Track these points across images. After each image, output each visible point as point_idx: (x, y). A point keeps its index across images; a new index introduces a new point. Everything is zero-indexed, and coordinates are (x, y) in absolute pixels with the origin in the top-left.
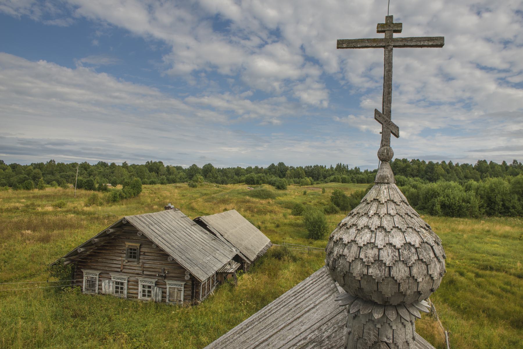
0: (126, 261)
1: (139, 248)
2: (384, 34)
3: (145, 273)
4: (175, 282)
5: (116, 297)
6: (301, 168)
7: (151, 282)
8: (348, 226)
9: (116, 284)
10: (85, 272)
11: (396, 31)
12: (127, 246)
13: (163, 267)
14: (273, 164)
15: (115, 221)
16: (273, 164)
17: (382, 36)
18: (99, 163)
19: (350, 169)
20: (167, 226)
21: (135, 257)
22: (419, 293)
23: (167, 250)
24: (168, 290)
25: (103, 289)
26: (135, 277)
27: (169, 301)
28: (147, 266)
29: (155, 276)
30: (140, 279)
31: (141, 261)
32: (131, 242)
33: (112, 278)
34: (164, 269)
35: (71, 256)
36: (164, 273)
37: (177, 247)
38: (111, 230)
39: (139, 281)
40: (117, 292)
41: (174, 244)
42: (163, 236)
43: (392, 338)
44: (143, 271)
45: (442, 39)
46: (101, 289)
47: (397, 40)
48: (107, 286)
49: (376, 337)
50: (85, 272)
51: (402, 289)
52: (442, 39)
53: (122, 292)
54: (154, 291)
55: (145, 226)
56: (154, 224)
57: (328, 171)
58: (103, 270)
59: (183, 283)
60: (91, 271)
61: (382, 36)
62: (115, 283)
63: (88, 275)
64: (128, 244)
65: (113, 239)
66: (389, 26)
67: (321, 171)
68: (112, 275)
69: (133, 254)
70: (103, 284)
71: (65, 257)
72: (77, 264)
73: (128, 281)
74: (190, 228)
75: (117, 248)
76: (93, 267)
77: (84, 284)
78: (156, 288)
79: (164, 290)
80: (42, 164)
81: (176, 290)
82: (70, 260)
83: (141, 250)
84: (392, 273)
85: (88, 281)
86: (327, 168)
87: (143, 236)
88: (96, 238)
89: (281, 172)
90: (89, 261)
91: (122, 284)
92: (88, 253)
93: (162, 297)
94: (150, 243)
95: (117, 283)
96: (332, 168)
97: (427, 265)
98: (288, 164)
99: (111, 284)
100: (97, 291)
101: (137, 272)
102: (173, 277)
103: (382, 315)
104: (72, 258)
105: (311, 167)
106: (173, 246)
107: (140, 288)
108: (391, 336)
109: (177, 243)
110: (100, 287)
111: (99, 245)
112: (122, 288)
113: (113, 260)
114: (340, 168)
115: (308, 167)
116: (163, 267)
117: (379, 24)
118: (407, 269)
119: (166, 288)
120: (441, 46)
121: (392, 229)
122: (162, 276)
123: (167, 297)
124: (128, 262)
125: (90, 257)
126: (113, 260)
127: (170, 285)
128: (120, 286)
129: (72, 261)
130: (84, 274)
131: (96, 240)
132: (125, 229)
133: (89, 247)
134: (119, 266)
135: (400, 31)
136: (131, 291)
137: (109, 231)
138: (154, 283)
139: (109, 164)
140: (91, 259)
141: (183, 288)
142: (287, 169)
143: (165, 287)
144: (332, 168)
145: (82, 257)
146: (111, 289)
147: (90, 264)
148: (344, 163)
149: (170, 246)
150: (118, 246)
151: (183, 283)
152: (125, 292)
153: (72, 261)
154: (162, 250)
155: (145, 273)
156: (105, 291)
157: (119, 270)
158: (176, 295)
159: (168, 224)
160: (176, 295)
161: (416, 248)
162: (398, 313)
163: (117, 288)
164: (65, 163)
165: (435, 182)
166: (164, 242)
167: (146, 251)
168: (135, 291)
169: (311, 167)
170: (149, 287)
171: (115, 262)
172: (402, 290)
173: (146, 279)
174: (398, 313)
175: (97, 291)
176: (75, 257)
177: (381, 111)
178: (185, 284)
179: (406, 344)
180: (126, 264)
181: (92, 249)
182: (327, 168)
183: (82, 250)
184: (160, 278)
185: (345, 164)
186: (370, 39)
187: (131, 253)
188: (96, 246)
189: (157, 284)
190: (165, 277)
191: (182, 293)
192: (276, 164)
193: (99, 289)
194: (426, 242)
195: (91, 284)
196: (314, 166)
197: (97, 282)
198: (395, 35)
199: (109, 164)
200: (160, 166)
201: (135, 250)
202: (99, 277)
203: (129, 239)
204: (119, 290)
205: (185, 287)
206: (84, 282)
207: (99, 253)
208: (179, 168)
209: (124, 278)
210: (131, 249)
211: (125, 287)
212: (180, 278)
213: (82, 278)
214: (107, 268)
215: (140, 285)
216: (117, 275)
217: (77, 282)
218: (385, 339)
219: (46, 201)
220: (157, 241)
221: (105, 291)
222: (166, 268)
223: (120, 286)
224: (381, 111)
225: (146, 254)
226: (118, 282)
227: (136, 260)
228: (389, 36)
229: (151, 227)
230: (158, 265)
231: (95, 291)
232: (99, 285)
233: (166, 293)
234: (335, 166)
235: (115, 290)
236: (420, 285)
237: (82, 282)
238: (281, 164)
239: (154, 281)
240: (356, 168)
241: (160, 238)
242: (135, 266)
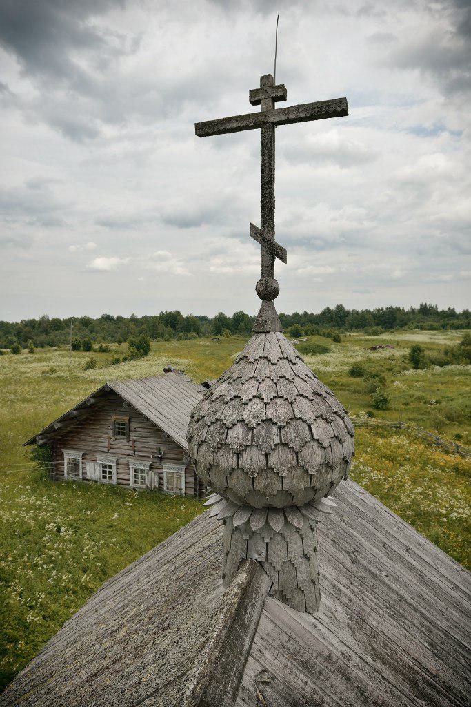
0: (114, 438)
1: (127, 422)
5: (103, 484)
6: (368, 312)
8: (214, 399)
10: (66, 452)
11: (275, 99)
14: (328, 309)
16: (328, 309)
17: (257, 109)
18: (103, 317)
21: (123, 434)
22: (315, 490)
24: (165, 474)
25: (88, 474)
27: (168, 489)
29: (149, 457)
30: (131, 460)
31: (131, 439)
32: (119, 415)
35: (49, 433)
36: (160, 453)
38: (92, 401)
40: (104, 477)
41: (170, 417)
45: (343, 101)
47: (282, 111)
48: (92, 470)
49: (243, 550)
50: (66, 452)
51: (258, 487)
52: (343, 101)
53: (110, 478)
55: (134, 395)
59: (184, 467)
60: (72, 452)
61: (257, 109)
63: (69, 455)
64: (114, 417)
67: (398, 315)
68: (98, 456)
69: (122, 430)
70: (88, 468)
72: (56, 440)
73: (117, 464)
75: (102, 422)
76: (75, 447)
77: (66, 468)
79: (161, 476)
82: (46, 438)
83: (131, 425)
84: (240, 462)
87: (130, 406)
88: (75, 410)
91: (110, 467)
92: (68, 429)
93: (159, 484)
95: (104, 466)
97: (297, 453)
98: (348, 307)
99: (97, 467)
101: (126, 452)
102: (171, 459)
105: (382, 309)
106: (168, 419)
107: (132, 473)
108: (264, 551)
110: (84, 471)
112: (110, 473)
114: (425, 311)
115: (378, 310)
118: (263, 458)
119: (163, 473)
120: (344, 113)
125: (71, 434)
127: (168, 469)
128: (107, 470)
129: (50, 439)
132: (107, 399)
133: (68, 422)
134: (105, 445)
135: (283, 98)
136: (121, 476)
138: (148, 466)
140: (72, 437)
142: (347, 313)
143: (161, 471)
146: (97, 473)
147: (70, 443)
148: (431, 302)
149: (164, 419)
150: (103, 420)
152: (114, 477)
153: (50, 439)
154: (155, 425)
157: (106, 450)
158: (175, 483)
159: (165, 391)
160: (175, 483)
161: (280, 428)
163: (104, 472)
164: (184, 314)
166: (157, 414)
167: (137, 426)
168: (125, 477)
169: (382, 309)
170: (142, 471)
171: (100, 440)
172: (259, 488)
177: (259, 226)
179: (288, 564)
180: (114, 443)
182: (406, 310)
183: (59, 425)
184: (155, 460)
186: (239, 117)
187: (119, 428)
189: (151, 467)
190: (161, 459)
191: (183, 479)
192: (333, 308)
193: (83, 474)
195: (74, 468)
197: (81, 465)
198: (279, 105)
201: (123, 424)
204: (107, 475)
205: (186, 472)
206: (65, 465)
207: (81, 428)
208: (203, 319)
209: (110, 460)
210: (119, 424)
211: (114, 470)
212: (178, 460)
215: (131, 469)
216: (103, 456)
218: (256, 556)
219: (30, 364)
220: (147, 413)
223: (107, 470)
224: (259, 226)
226: (106, 466)
228: (270, 110)
229: (142, 396)
230: (152, 444)
231: (78, 475)
232: (83, 469)
234: (417, 307)
237: (63, 465)
238: (340, 308)
239: (148, 464)
240: (449, 309)
241: (152, 409)
242: (123, 445)
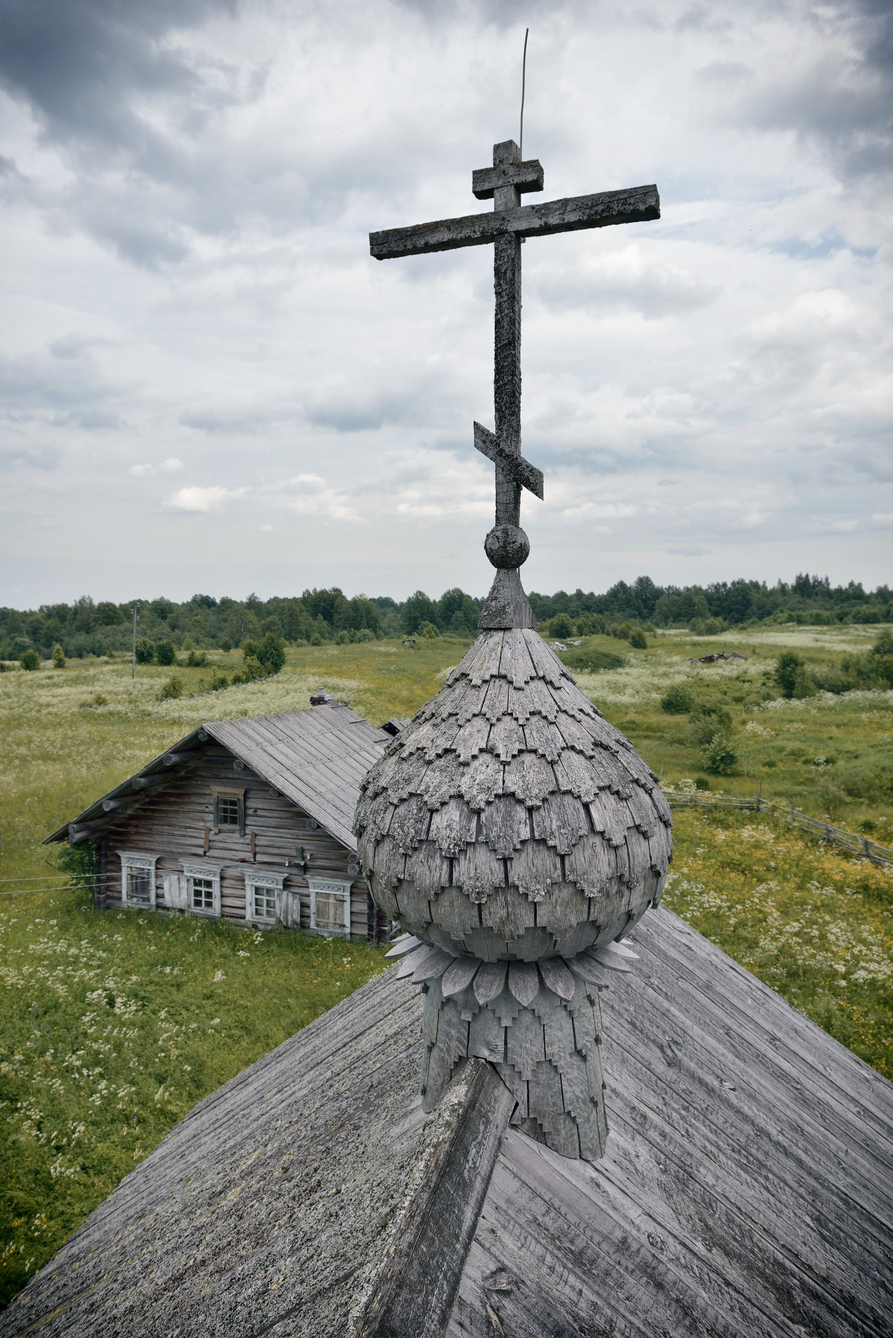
1: (242, 798)
2: (491, 201)
3: (259, 858)
4: (330, 882)
6: (697, 590)
9: (196, 884)
10: (124, 856)
12: (215, 795)
13: (300, 843)
15: (179, 735)
16: (622, 585)
17: (488, 206)
18: (194, 600)
19: (833, 586)
20: (308, 744)
21: (234, 821)
23: (306, 804)
25: (167, 896)
26: (237, 866)
27: (318, 925)
29: (283, 865)
30: (248, 871)
31: (248, 830)
33: (185, 869)
34: (303, 850)
35: (92, 819)
36: (304, 858)
37: (330, 796)
38: (175, 758)
39: (246, 878)
40: (198, 903)
42: (299, 772)
43: (501, 1048)
44: (255, 854)
45: (651, 191)
46: (162, 896)
48: (175, 888)
49: (461, 1042)
50: (124, 856)
52: (651, 191)
53: (209, 904)
54: (280, 900)
55: (254, 747)
56: (275, 740)
57: (772, 592)
58: (163, 851)
61: (488, 206)
62: (192, 881)
63: (131, 862)
64: (217, 790)
65: (184, 778)
66: (509, 172)
67: (755, 596)
69: (231, 814)
70: (166, 885)
71: (76, 823)
73: (222, 878)
74: (369, 749)
75: (193, 799)
76: (141, 845)
78: (285, 893)
79: (305, 900)
80: (64, 607)
81: (332, 901)
82: (88, 828)
84: (455, 875)
85: (132, 876)
87: (247, 769)
89: (644, 601)
90: (133, 830)
91: (209, 884)
92: (129, 812)
93: (302, 916)
94: (265, 786)
95: (198, 883)
97: (562, 857)
98: (660, 582)
99: (184, 884)
100: (153, 901)
101: (242, 855)
103: (500, 991)
104: (92, 823)
105: (725, 585)
106: (319, 794)
107: (250, 895)
109: (332, 786)
110: (160, 891)
111: (154, 794)
112: (209, 895)
113: (187, 827)
115: (717, 587)
116: (300, 843)
117: (475, 172)
118: (497, 867)
119: (308, 896)
120: (653, 213)
121: (474, 757)
122: (298, 866)
123: (312, 916)
124: (220, 832)
126: (187, 827)
130: (123, 860)
131: (142, 780)
132: (203, 755)
133: (129, 799)
135: (536, 186)
136: (229, 901)
137: (169, 758)
138: (281, 882)
139: (218, 601)
140: (136, 826)
141: (347, 894)
143: (305, 891)
145: (116, 821)
146: (184, 895)
147: (135, 838)
148: (816, 571)
149: (311, 793)
150: (194, 794)
152: (216, 902)
153: (94, 830)
154: (293, 804)
155: (259, 858)
156: (172, 902)
157: (200, 851)
158: (332, 912)
160: (332, 912)
161: (530, 810)
162: (542, 982)
163: (198, 893)
167: (260, 806)
168: (237, 902)
169: (725, 585)
170: (269, 891)
171: (190, 832)
172: (490, 924)
173: (261, 874)
174: (542, 982)
175: (153, 901)
176: (99, 821)
178: (352, 887)
181: (136, 801)
183: (112, 804)
184: (295, 871)
188: (147, 796)
190: (305, 869)
191: (347, 905)
194: (569, 792)
195: (140, 885)
197: (153, 880)
198: (528, 199)
199: (218, 601)
200: (336, 597)
201: (233, 803)
202: (157, 868)
203: (218, 777)
205: (352, 894)
207: (153, 811)
209: (208, 871)
211: (216, 890)
212: (338, 871)
213: (119, 870)
215: (248, 888)
217: (109, 879)
218: (485, 1053)
221: (172, 902)
222: (306, 847)
223: (203, 889)
225: (259, 813)
226: (200, 881)
227: (237, 827)
229: (269, 749)
230: (288, 841)
231: (148, 900)
232: (157, 888)
233: (308, 907)
234: (791, 581)
235: (193, 898)
236: (541, 911)
237: (119, 879)
238: (644, 582)
239: (281, 877)
240: (851, 584)
241: (288, 775)
242: (233, 841)
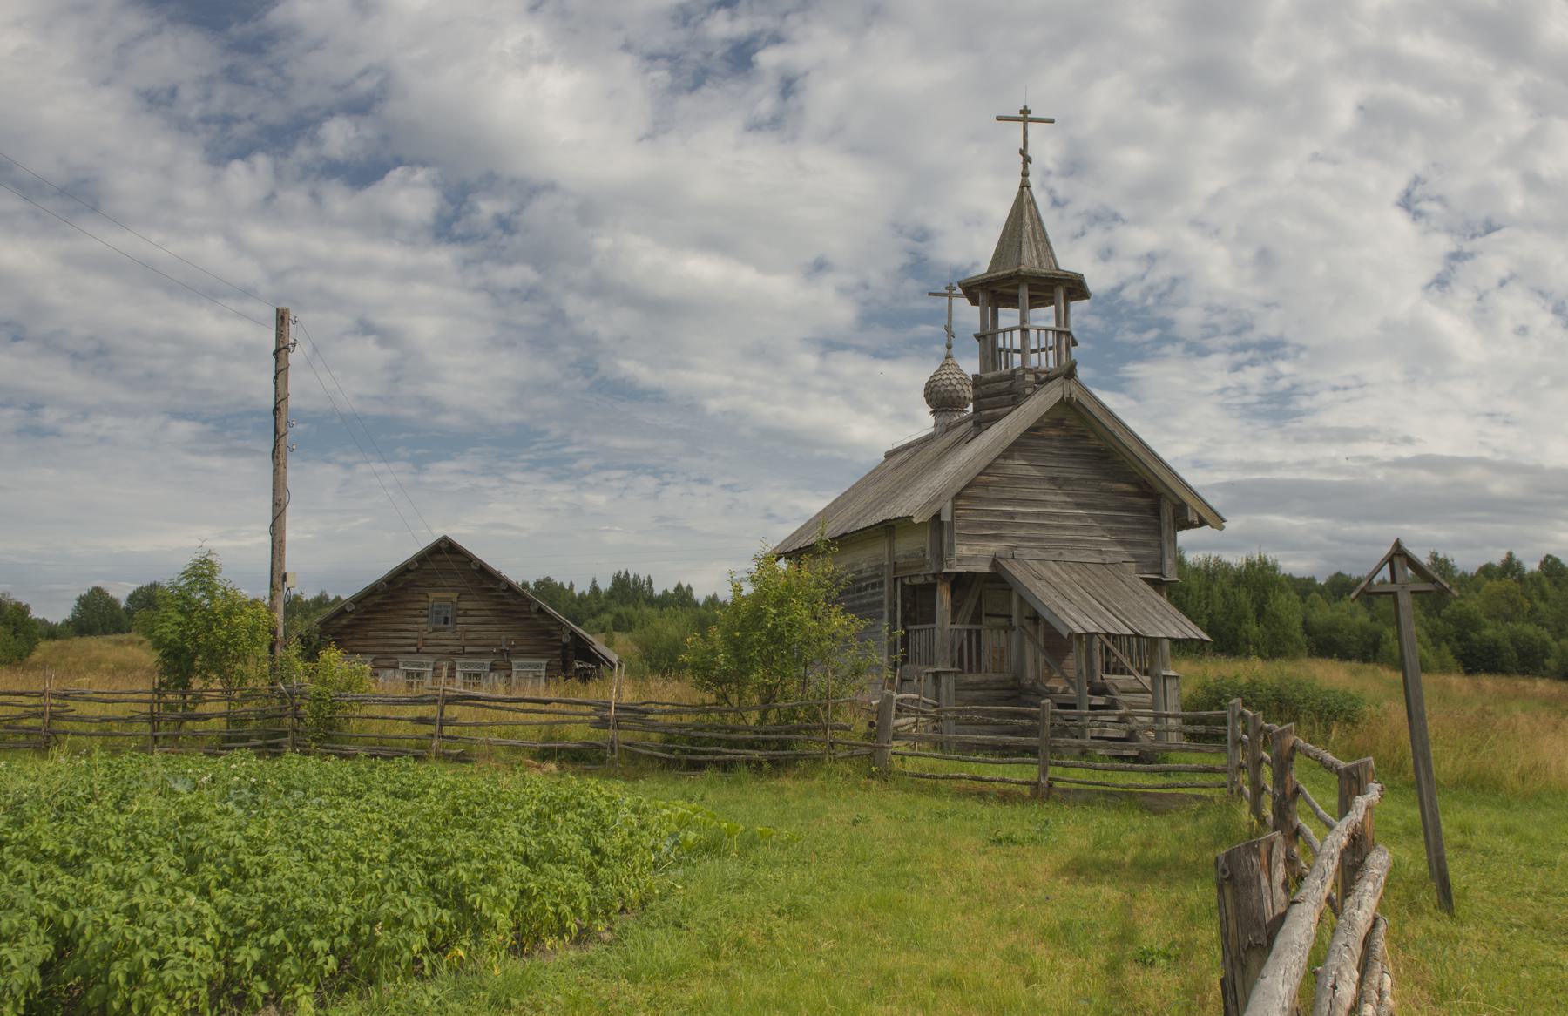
3: (468, 649)
7: (482, 665)
19: (658, 591)
28: (472, 635)
59: (544, 662)
66: (1025, 111)
68: (402, 659)
86: (577, 591)
96: (595, 589)
101: (452, 648)
124: (435, 630)
144: (595, 589)
148: (639, 570)
151: (544, 662)
165: (1070, 398)
182: (577, 591)
185: (643, 577)
190: (509, 654)
196: (538, 584)
214: (387, 649)
234: (605, 585)
239: (488, 662)
240: (679, 587)
